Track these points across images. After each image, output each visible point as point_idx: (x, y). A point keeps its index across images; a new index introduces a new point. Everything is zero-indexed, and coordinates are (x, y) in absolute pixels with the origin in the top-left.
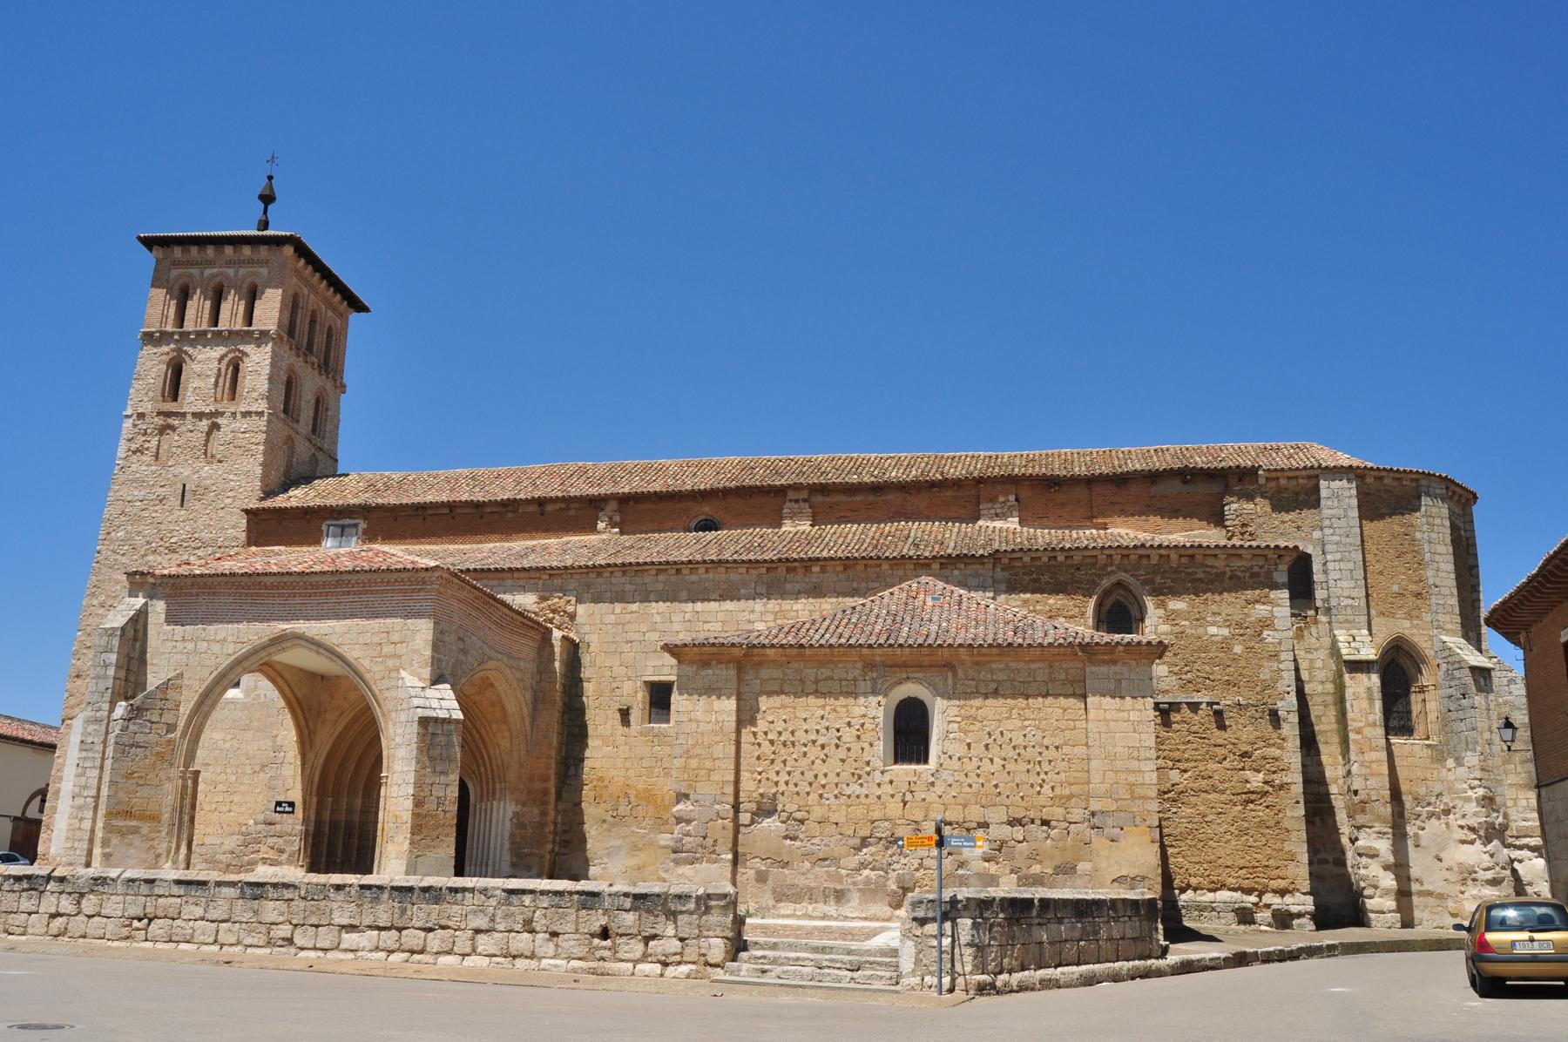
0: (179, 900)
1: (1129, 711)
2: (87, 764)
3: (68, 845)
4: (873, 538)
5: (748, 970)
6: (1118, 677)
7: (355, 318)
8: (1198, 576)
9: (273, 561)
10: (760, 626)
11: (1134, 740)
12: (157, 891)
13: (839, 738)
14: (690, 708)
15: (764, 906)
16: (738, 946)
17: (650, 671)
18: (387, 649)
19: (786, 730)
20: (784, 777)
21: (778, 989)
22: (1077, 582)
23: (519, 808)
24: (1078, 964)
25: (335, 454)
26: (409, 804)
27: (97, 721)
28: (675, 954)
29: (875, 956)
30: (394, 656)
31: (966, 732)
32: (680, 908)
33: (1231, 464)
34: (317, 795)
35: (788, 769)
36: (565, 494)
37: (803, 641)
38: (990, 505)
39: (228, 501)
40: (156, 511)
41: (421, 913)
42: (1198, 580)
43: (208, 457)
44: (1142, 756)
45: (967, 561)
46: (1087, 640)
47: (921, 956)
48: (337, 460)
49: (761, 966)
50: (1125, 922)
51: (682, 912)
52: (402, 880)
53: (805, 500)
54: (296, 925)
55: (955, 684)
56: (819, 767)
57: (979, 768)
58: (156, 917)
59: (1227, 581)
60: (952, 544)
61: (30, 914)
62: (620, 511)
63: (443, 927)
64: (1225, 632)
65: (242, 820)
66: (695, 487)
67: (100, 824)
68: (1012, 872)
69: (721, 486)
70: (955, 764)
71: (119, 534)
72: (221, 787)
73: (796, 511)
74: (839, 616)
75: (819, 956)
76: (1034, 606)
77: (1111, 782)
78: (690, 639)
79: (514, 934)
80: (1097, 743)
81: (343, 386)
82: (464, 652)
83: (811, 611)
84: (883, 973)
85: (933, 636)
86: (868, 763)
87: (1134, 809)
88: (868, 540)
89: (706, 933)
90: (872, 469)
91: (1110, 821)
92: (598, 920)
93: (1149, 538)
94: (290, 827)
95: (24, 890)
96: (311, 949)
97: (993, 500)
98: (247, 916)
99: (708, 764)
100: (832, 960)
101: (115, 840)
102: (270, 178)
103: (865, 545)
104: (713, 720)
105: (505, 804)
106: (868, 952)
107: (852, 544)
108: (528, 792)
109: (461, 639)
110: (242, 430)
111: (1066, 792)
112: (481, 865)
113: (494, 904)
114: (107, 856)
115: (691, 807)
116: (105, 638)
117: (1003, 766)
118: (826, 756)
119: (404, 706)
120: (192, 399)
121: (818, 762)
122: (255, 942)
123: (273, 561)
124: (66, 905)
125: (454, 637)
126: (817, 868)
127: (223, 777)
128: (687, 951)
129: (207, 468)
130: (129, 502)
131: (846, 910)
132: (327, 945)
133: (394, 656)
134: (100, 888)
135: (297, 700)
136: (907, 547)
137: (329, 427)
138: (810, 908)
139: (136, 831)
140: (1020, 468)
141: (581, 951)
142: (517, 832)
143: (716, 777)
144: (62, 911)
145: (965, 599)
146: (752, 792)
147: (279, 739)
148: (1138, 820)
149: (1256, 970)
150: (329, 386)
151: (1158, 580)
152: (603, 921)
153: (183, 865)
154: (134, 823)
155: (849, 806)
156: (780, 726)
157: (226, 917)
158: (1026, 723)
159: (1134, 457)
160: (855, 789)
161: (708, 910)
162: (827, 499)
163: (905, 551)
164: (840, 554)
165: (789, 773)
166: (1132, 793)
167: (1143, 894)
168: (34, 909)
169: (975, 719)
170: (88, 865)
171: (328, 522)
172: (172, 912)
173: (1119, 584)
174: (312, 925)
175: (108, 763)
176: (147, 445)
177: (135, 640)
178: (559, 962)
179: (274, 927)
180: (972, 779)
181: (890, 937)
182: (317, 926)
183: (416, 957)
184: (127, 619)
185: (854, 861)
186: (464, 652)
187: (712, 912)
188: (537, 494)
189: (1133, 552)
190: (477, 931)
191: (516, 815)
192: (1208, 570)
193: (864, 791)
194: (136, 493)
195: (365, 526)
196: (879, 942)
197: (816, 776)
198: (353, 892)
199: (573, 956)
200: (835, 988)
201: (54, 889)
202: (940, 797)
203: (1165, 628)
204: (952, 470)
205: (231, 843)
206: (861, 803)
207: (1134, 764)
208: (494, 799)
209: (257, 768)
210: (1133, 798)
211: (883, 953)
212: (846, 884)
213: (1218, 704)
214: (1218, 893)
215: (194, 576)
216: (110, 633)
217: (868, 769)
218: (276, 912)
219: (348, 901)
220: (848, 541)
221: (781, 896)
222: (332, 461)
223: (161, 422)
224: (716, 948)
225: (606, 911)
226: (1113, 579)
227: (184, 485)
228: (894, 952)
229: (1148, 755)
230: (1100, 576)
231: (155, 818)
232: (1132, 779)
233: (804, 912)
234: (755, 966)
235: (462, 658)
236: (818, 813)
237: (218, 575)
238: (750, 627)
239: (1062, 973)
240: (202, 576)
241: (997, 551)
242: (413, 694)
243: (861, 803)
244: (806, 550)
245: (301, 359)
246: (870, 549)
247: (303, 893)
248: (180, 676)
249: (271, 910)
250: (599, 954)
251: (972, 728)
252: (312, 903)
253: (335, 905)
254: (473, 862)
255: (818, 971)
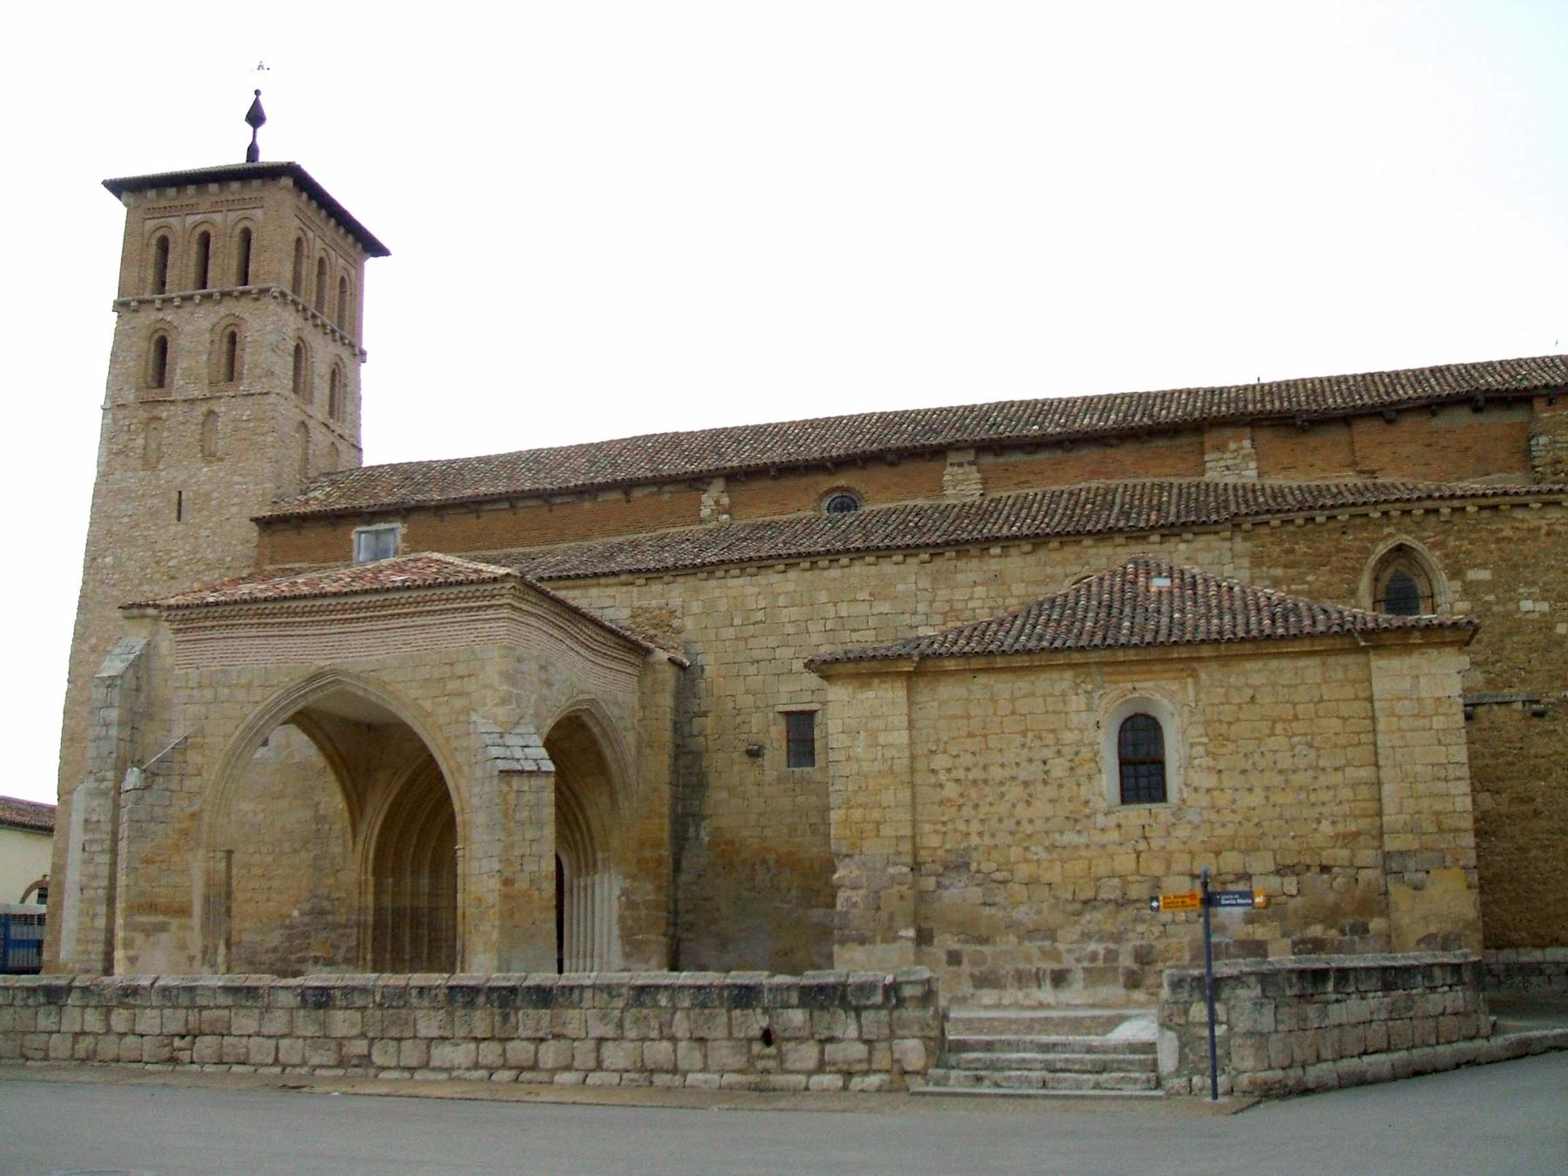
0: (226, 1012)
1: (1431, 716)
2: (96, 848)
3: (80, 948)
4: (1066, 508)
5: (957, 1078)
6: (1415, 672)
7: (372, 265)
8: (1504, 534)
9: (300, 581)
10: (924, 631)
11: (1439, 755)
12: (200, 1001)
13: (1046, 772)
14: (848, 743)
15: (960, 994)
16: (942, 1050)
17: (784, 698)
18: (453, 686)
19: (975, 765)
20: (975, 827)
21: (1000, 1101)
22: (1344, 550)
23: (627, 884)
24: (1388, 1050)
25: (359, 442)
26: (495, 883)
27: (104, 794)
28: (860, 1061)
29: (1123, 1053)
30: (460, 694)
31: (1215, 756)
32: (863, 1002)
33: (1536, 382)
34: (374, 873)
35: (981, 816)
36: (654, 473)
37: (992, 647)
38: (1217, 455)
39: (234, 510)
40: (148, 528)
41: (529, 1020)
42: (1504, 539)
43: (209, 456)
44: (1451, 775)
45: (1196, 529)
46: (1371, 625)
47: (1187, 1050)
48: (361, 450)
49: (974, 1073)
50: (1445, 992)
51: (867, 1008)
52: (500, 980)
53: (971, 463)
54: (373, 1039)
55: (1197, 695)
56: (1022, 811)
57: (1234, 802)
58: (202, 1034)
59: (1543, 539)
60: (1173, 509)
61: (50, 1033)
62: (727, 490)
63: (557, 1037)
64: (1544, 607)
65: (284, 910)
66: (825, 454)
67: (119, 921)
68: (1284, 935)
69: (858, 451)
70: (1204, 800)
71: (107, 560)
72: (257, 871)
73: (960, 478)
74: (1034, 612)
75: (1050, 1056)
76: (1289, 586)
77: (1411, 811)
78: (841, 652)
79: (648, 1043)
80: (1391, 762)
81: (363, 353)
82: (549, 684)
83: (991, 608)
84: (1137, 1075)
85: (1164, 631)
86: (1087, 802)
87: (1442, 846)
88: (1060, 511)
89: (899, 1032)
90: (1057, 417)
91: (1411, 864)
92: (757, 1022)
93: (1433, 487)
94: (345, 918)
95: (40, 1005)
96: (395, 1068)
97: (1221, 448)
98: (311, 1030)
99: (876, 815)
100: (1067, 1060)
101: (139, 938)
102: (257, 93)
103: (1057, 518)
104: (879, 757)
105: (610, 880)
106: (1115, 1049)
107: (1040, 517)
108: (639, 862)
109: (543, 668)
110: (245, 418)
111: (1353, 828)
112: (585, 956)
113: (621, 1004)
114: (132, 960)
115: (857, 872)
116: (103, 690)
117: (1267, 798)
118: (1030, 796)
119: (479, 757)
120: (181, 382)
121: (1021, 806)
122: (325, 1060)
123: (300, 581)
124: (93, 1021)
125: (534, 666)
126: (1027, 943)
127: (256, 858)
128: (877, 1055)
129: (205, 470)
130: (116, 517)
131: (1065, 996)
132: (414, 1063)
133: (460, 694)
134: (131, 1000)
135: (341, 756)
136: (1113, 516)
137: (350, 408)
138: (1020, 996)
139: (163, 928)
140: (1255, 403)
141: (740, 1061)
142: (626, 913)
143: (887, 831)
144: (87, 1029)
145: (1200, 581)
146: (935, 849)
147: (322, 806)
148: (1449, 860)
149: (578, 1108)
150: (345, 354)
151: (1452, 542)
152: (764, 1022)
153: (223, 968)
154: (161, 918)
155: (1063, 861)
156: (967, 760)
157: (284, 1030)
158: (1296, 739)
159: (1404, 381)
160: (1070, 838)
161: (901, 1002)
162: (1001, 460)
163: (1112, 522)
164: (1025, 531)
165: (982, 821)
166: (1439, 824)
167: (1465, 955)
168: (55, 1028)
169: (1228, 739)
170: (108, 970)
171: (359, 529)
172: (220, 1028)
173: (1400, 549)
174: (392, 1039)
175: (123, 845)
176: (132, 444)
177: (1495, 508)
178: (707, 1076)
179: (344, 1042)
180: (1227, 816)
181: (1138, 1028)
182: (399, 1040)
183: (526, 1076)
184: (127, 664)
185: (1073, 932)
186: (549, 684)
187: (908, 1004)
188: (620, 476)
189: (1417, 504)
190: (601, 1040)
191: (625, 892)
192: (1517, 525)
193: (1082, 840)
194: (123, 507)
195: (404, 531)
196: (1127, 1032)
197: (1018, 823)
198: (441, 997)
199: (727, 1068)
200: (1076, 1097)
201: (78, 1003)
202: (1185, 843)
203: (1463, 606)
204: (1164, 412)
205: (275, 938)
206: (1080, 857)
207: (1441, 786)
208: (595, 873)
209: (297, 845)
210: (1441, 830)
211: (1133, 1048)
212: (1068, 962)
213: (1537, 702)
214: (1548, 950)
215: (208, 605)
216: (110, 683)
217: (1087, 811)
218: (346, 1024)
219: (434, 1008)
220: (1033, 513)
221: (985, 981)
222: (353, 451)
223: (146, 415)
224: (912, 1051)
225: (766, 1011)
226: (1392, 543)
227: (180, 493)
228: (1150, 1047)
229: (1458, 774)
230: (1374, 541)
231: (183, 911)
232: (1438, 807)
233: (1012, 1000)
234: (967, 1073)
235: (545, 691)
236: (1023, 871)
237: (236, 602)
238: (911, 634)
239: (1370, 1064)
240: (217, 604)
241: (1236, 514)
242: (489, 742)
243: (1080, 857)
244: (979, 527)
245: (310, 322)
246: (1064, 521)
247: (378, 998)
248: (201, 732)
249: (342, 1022)
250: (760, 1064)
251: (1223, 751)
252: (390, 1011)
253: (419, 1013)
254: (574, 953)
255: (1051, 1075)
